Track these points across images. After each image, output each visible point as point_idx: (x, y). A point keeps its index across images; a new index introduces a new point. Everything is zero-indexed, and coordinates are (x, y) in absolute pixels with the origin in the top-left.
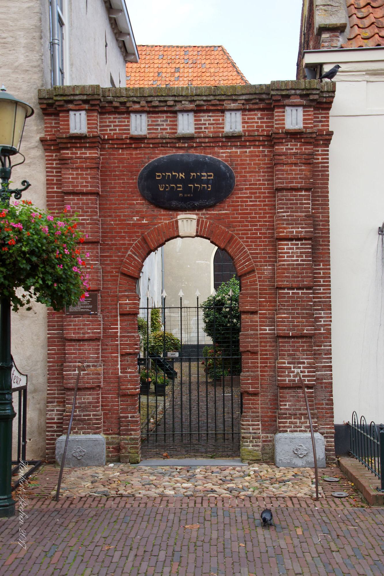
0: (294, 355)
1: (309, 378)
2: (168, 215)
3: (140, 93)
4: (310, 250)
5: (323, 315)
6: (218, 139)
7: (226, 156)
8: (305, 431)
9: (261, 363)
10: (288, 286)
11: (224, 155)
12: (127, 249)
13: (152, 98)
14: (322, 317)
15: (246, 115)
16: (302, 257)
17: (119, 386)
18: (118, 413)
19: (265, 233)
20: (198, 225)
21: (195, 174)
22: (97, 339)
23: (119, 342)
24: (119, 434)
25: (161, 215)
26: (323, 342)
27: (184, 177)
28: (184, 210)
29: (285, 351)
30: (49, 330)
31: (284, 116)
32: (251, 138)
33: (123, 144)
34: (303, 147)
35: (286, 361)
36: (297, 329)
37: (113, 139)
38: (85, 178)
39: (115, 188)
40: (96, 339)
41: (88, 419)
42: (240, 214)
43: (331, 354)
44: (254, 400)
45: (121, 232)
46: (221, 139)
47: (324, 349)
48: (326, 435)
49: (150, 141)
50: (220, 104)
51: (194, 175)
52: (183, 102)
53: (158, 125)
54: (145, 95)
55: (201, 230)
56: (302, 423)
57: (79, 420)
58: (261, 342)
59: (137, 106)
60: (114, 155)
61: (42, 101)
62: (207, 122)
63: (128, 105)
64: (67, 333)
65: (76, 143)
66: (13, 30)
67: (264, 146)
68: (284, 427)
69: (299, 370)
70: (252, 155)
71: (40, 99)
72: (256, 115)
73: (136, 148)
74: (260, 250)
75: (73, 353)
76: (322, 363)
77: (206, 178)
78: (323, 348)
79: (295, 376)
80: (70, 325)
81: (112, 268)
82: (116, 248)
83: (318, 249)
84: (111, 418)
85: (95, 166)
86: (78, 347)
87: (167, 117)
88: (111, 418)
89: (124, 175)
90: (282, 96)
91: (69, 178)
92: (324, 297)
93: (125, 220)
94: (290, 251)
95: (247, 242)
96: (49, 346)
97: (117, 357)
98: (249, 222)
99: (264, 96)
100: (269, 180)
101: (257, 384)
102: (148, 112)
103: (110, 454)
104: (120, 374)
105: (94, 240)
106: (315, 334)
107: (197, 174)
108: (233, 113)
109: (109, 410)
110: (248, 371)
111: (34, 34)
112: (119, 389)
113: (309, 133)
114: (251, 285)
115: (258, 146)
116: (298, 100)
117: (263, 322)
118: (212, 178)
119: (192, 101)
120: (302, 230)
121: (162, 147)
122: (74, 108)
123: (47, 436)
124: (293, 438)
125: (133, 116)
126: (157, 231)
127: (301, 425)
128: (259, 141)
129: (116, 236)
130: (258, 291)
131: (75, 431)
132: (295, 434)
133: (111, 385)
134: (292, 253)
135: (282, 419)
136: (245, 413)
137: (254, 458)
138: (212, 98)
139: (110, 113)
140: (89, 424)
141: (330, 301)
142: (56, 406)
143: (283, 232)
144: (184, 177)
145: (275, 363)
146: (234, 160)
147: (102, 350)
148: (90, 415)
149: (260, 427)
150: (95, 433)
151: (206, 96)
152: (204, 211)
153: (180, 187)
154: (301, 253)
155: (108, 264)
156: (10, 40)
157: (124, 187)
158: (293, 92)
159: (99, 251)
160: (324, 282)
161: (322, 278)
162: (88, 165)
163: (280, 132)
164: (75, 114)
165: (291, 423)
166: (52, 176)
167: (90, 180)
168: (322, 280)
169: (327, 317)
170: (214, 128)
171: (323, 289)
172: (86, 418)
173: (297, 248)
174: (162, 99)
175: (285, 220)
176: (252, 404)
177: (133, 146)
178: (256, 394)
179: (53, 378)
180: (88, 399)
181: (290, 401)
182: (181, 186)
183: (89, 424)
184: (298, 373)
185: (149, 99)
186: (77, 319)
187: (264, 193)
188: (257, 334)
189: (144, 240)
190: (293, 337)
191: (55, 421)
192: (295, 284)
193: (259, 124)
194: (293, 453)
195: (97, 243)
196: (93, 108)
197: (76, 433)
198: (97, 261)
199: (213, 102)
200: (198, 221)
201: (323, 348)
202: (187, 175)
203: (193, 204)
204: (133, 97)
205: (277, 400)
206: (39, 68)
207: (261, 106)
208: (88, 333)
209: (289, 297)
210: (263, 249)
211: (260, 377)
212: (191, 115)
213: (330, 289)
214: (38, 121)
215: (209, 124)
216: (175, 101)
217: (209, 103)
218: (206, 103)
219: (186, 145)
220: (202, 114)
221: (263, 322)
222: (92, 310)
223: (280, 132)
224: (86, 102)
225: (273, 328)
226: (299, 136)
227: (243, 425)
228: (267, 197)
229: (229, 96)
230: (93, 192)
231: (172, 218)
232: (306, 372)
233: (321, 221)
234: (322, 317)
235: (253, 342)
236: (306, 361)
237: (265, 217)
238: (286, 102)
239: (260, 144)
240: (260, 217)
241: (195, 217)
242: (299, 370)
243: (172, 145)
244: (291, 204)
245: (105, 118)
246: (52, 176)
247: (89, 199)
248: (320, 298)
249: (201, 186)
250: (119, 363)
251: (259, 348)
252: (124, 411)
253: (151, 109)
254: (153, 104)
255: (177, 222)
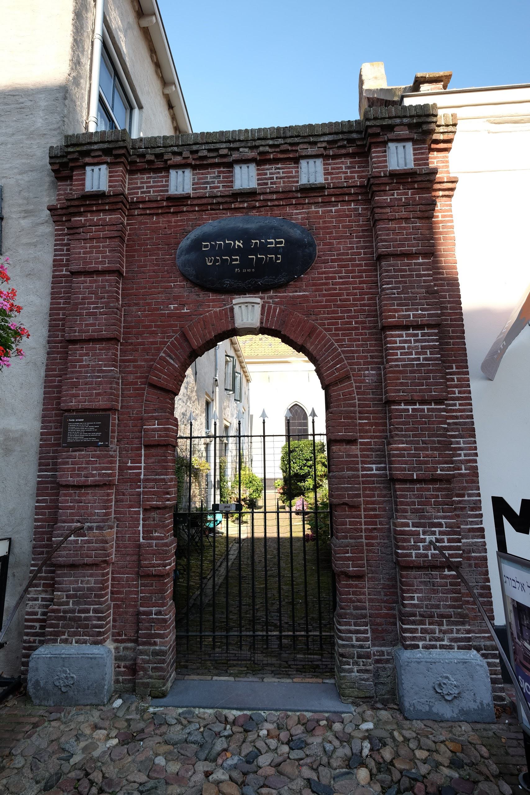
0: (423, 511)
1: (450, 552)
2: (218, 301)
3: (182, 141)
4: (437, 344)
5: (462, 445)
6: (291, 195)
7: (303, 219)
8: (451, 647)
9: (366, 523)
10: (406, 398)
11: (300, 216)
12: (159, 350)
13: (198, 146)
14: (461, 449)
15: (329, 164)
16: (426, 353)
17: (139, 560)
18: (135, 606)
19: (364, 322)
20: (262, 314)
21: (258, 241)
22: (108, 485)
23: (142, 489)
24: (136, 641)
25: (209, 301)
26: (465, 488)
27: (242, 246)
28: (242, 292)
29: (408, 504)
30: (40, 471)
31: (385, 156)
32: (337, 191)
33: (158, 208)
34: (417, 197)
35: (410, 522)
36: (426, 468)
37: (144, 202)
38: (101, 252)
39: (145, 266)
40: (105, 485)
41: (86, 619)
42: (324, 295)
43: (480, 508)
44: (356, 586)
45: (151, 326)
46: (296, 195)
47: (469, 501)
48: (484, 652)
49: (195, 202)
50: (292, 151)
51: (256, 243)
52: (241, 150)
53: (208, 183)
54: (189, 143)
55: (267, 320)
56: (445, 632)
57: (71, 619)
58: (365, 489)
59: (178, 159)
60: (146, 223)
61: (53, 161)
62: (275, 176)
63: (166, 157)
64: (61, 476)
65: (91, 205)
66: (33, 94)
67: (356, 201)
68: (414, 638)
69: (433, 538)
70: (340, 215)
71: (51, 157)
72: (342, 163)
73: (175, 213)
74: (357, 346)
75: (70, 506)
76: (467, 524)
77: (273, 246)
78: (466, 498)
79: (426, 548)
80: (67, 463)
81: (137, 378)
82: (144, 349)
83: (448, 344)
84: (126, 613)
85: (116, 234)
86: (77, 498)
87: (219, 172)
88: (126, 613)
89: (158, 249)
90: (383, 127)
91: (80, 253)
92: (462, 417)
93: (158, 309)
94: (406, 345)
95: (338, 335)
96: (38, 495)
97: (138, 513)
98: (339, 306)
99: (355, 136)
100: (366, 247)
101: (361, 559)
102: (194, 167)
103: (121, 678)
104: (141, 540)
105: (109, 336)
106: (454, 476)
107: (260, 241)
108: (311, 161)
109: (122, 600)
110: (345, 537)
111: (58, 95)
112: (139, 566)
113: (425, 174)
114: (345, 400)
115: (349, 202)
116: (404, 132)
117: (368, 456)
118: (283, 245)
119: (252, 148)
120: (423, 313)
121: (212, 209)
122: (92, 162)
123: (25, 642)
124: (431, 663)
125: (173, 172)
126: (202, 322)
127: (442, 635)
128: (349, 194)
129: (143, 333)
130: (357, 409)
131: (63, 637)
132: (435, 653)
133: (128, 559)
134: (409, 348)
135: (408, 624)
136: (342, 608)
137: (362, 694)
138: (281, 141)
139: (143, 171)
140: (86, 626)
141: (473, 423)
142: (40, 592)
143: (394, 317)
144: (242, 246)
145: (389, 523)
146: (314, 223)
147: (116, 501)
148: (88, 611)
149: (369, 635)
150: (96, 643)
151: (272, 139)
152: (272, 293)
153: (236, 260)
154: (423, 347)
155: (130, 372)
156: (29, 104)
157: (158, 265)
158: (398, 121)
159: (119, 353)
160: (460, 392)
161: (456, 386)
162: (106, 234)
163: (382, 175)
164: (93, 170)
165: (424, 631)
166: (61, 255)
167: (108, 254)
168: (456, 390)
169: (470, 449)
170: (284, 182)
171: (460, 405)
172: (83, 615)
173: (416, 341)
174: (212, 146)
175: (395, 299)
176: (354, 593)
177: (172, 210)
178: (359, 577)
179: (41, 547)
180: (88, 582)
181: (420, 591)
182: (238, 257)
183: (86, 626)
184: (431, 542)
185: (195, 148)
186: (77, 453)
187: (360, 265)
188: (358, 477)
189: (184, 336)
190: (419, 481)
191: (39, 617)
192: (416, 396)
193: (349, 174)
194: (432, 692)
195: (115, 340)
196: (118, 160)
197: (66, 641)
198: (115, 366)
199: (283, 147)
200: (263, 307)
201: (466, 498)
202: (247, 243)
203: (256, 282)
204: (172, 146)
205: (395, 586)
206: (58, 131)
207: (351, 150)
208: (93, 476)
209: (408, 416)
210: (362, 345)
211: (365, 548)
212: (253, 167)
213: (471, 404)
214: (52, 191)
215: (277, 178)
216: (230, 149)
217: (278, 150)
218: (273, 150)
219: (246, 205)
220: (267, 167)
221: (368, 456)
222: (100, 438)
223: (382, 175)
224: (107, 152)
225: (383, 465)
226: (410, 180)
227: (340, 631)
228: (365, 271)
229: (304, 137)
230: (111, 269)
231: (225, 305)
232: (446, 540)
233: (449, 302)
234: (461, 449)
235: (351, 489)
236: (443, 521)
237: (363, 299)
238: (391, 136)
239: (351, 198)
240: (354, 300)
241: (258, 300)
242: (434, 537)
243: (226, 206)
244: (402, 276)
245: (136, 179)
246: (61, 255)
247: (107, 281)
248: (456, 417)
249: (266, 257)
250: (141, 522)
251: (362, 499)
252: (146, 602)
253: (198, 163)
254: (200, 154)
255: (232, 309)
